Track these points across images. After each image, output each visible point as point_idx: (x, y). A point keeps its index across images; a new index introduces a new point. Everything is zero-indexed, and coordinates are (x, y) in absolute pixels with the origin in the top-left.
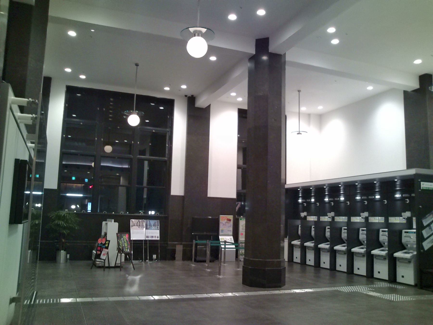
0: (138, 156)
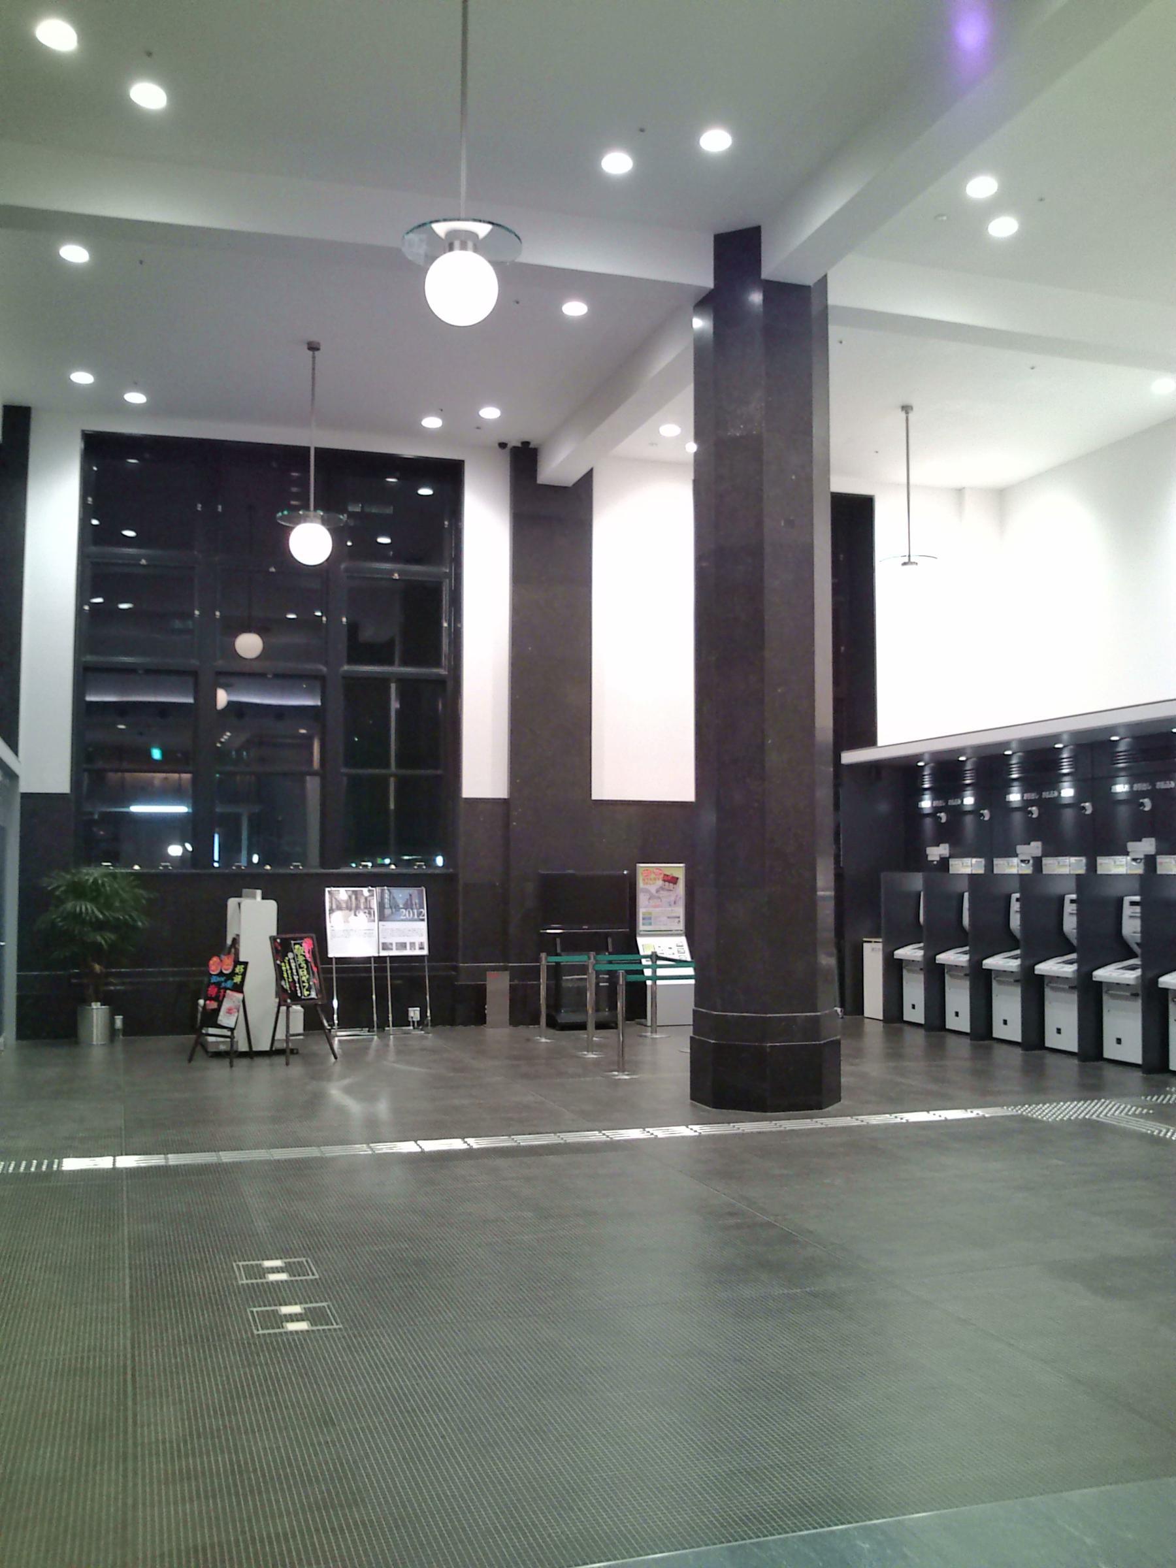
0: (346, 668)
